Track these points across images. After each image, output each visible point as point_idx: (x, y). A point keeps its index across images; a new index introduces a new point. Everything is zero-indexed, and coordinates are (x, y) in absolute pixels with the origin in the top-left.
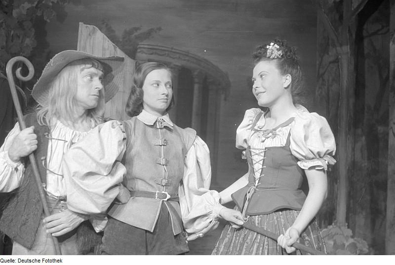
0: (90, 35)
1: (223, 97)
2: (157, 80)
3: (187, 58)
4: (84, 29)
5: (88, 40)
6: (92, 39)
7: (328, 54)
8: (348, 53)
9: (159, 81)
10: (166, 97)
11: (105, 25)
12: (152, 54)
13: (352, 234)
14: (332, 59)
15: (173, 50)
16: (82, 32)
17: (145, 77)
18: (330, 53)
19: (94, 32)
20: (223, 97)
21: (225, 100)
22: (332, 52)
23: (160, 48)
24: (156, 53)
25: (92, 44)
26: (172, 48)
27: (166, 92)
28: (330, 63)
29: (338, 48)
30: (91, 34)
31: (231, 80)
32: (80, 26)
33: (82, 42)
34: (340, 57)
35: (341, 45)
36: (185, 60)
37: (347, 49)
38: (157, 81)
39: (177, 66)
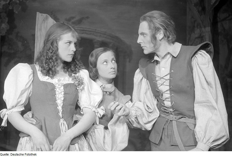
0: (44, 20)
1: (128, 60)
2: (70, 40)
3: (105, 36)
4: (40, 17)
5: (43, 24)
6: (46, 23)
7: (194, 33)
8: (209, 32)
9: (106, 60)
10: (114, 70)
11: (53, 14)
12: (83, 33)
13: (69, 59)
14: (197, 36)
15: (96, 31)
16: (38, 18)
17: (97, 59)
18: (196, 32)
19: (47, 18)
20: (128, 60)
21: (129, 62)
22: (197, 31)
23: (88, 30)
24: (85, 33)
25: (45, 26)
26: (96, 30)
27: (113, 67)
28: (196, 38)
29: (203, 29)
30: (45, 20)
31: (133, 49)
32: (37, 14)
33: (39, 25)
34: (204, 34)
35: (205, 27)
36: (104, 37)
37: (208, 29)
38: (105, 60)
39: (99, 41)
